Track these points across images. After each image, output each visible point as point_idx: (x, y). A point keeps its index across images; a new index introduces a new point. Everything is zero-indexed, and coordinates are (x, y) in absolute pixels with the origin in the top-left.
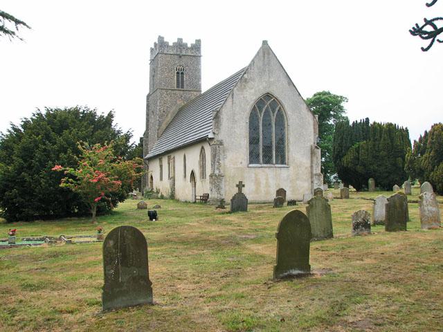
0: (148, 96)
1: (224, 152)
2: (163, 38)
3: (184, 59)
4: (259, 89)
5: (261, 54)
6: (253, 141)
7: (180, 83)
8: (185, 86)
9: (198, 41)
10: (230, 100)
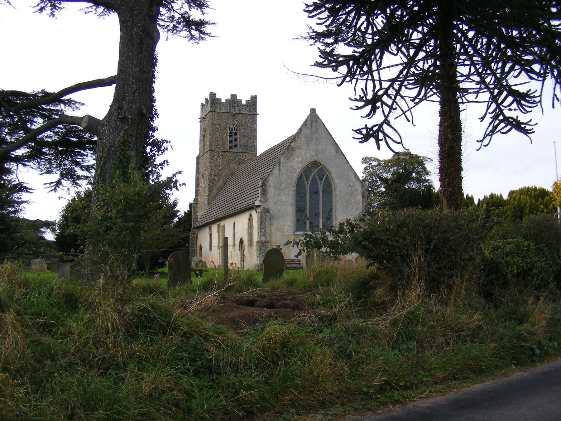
0: (198, 158)
1: (270, 219)
2: (215, 94)
3: (239, 119)
4: (307, 157)
5: (309, 123)
6: (300, 210)
7: (233, 145)
8: (238, 147)
9: (254, 99)
10: (277, 168)
